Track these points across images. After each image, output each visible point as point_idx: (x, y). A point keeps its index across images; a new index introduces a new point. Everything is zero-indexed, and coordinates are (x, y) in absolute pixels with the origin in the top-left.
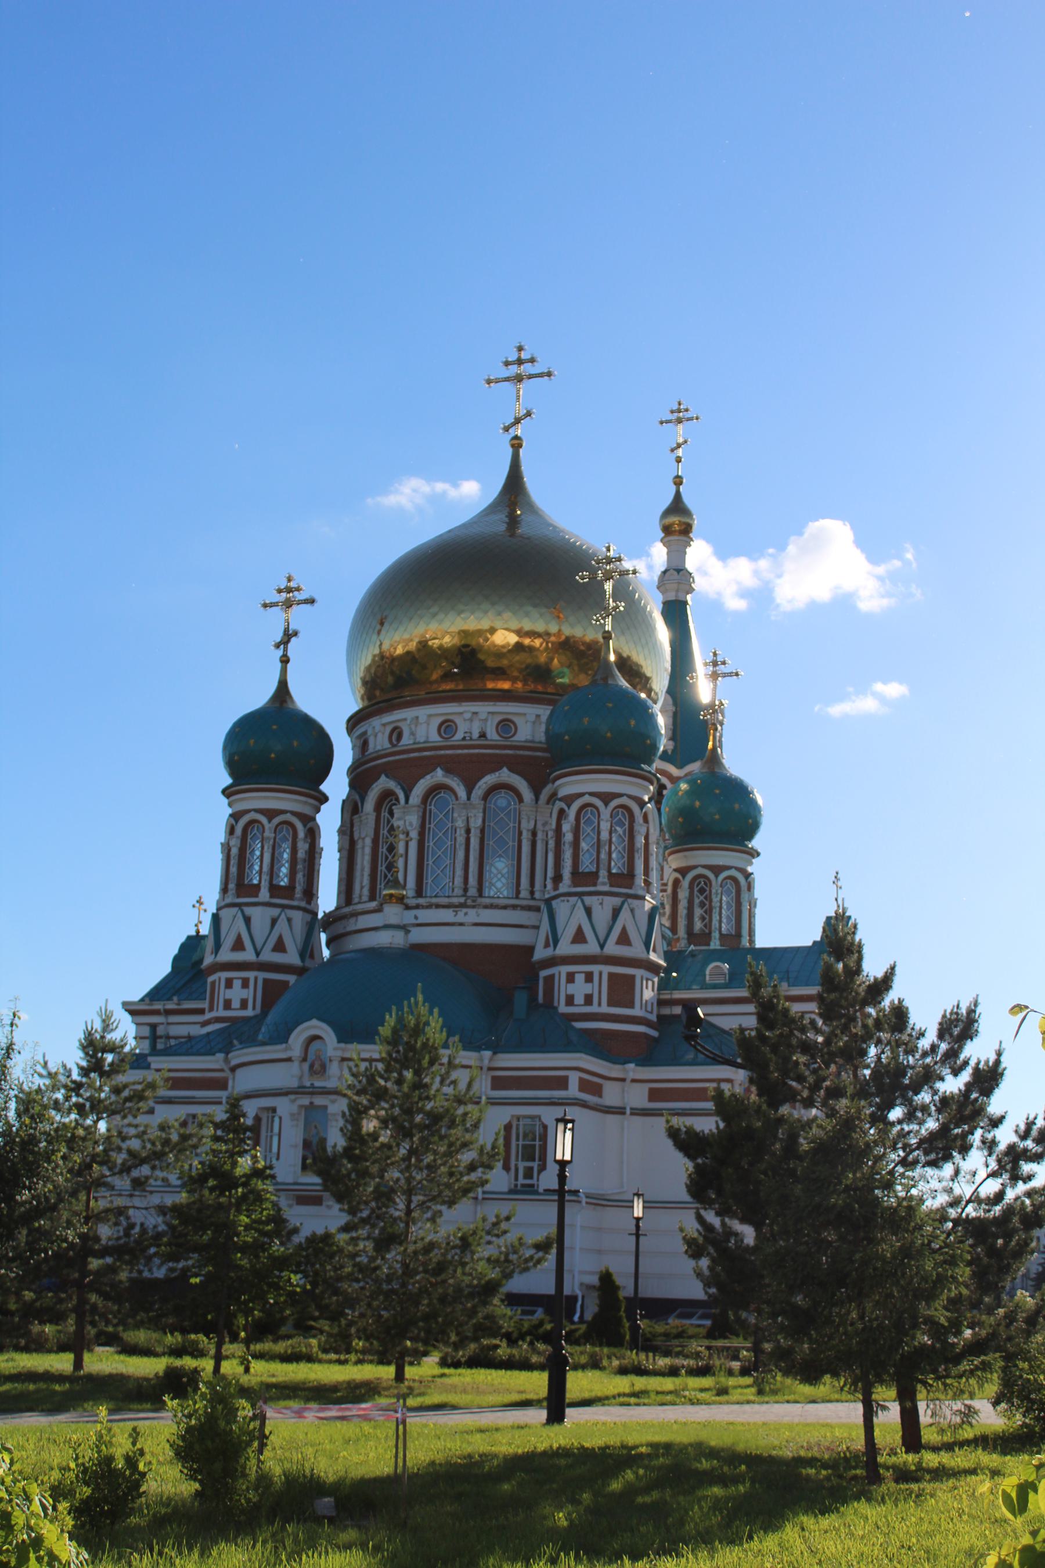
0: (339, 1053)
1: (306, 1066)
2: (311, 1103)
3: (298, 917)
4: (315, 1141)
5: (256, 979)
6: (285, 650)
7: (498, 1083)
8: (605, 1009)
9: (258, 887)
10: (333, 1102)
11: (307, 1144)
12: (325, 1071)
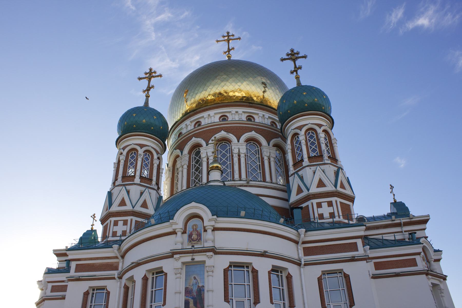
0: (213, 223)
1: (186, 236)
2: (193, 259)
3: (154, 193)
4: (195, 289)
5: (131, 220)
6: (148, 93)
7: (307, 252)
8: (309, 203)
9: (134, 176)
10: (211, 257)
11: (188, 292)
12: (200, 239)
